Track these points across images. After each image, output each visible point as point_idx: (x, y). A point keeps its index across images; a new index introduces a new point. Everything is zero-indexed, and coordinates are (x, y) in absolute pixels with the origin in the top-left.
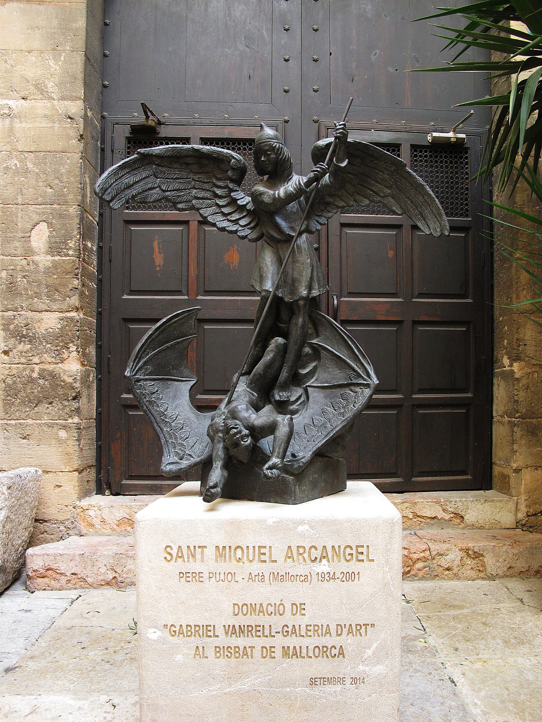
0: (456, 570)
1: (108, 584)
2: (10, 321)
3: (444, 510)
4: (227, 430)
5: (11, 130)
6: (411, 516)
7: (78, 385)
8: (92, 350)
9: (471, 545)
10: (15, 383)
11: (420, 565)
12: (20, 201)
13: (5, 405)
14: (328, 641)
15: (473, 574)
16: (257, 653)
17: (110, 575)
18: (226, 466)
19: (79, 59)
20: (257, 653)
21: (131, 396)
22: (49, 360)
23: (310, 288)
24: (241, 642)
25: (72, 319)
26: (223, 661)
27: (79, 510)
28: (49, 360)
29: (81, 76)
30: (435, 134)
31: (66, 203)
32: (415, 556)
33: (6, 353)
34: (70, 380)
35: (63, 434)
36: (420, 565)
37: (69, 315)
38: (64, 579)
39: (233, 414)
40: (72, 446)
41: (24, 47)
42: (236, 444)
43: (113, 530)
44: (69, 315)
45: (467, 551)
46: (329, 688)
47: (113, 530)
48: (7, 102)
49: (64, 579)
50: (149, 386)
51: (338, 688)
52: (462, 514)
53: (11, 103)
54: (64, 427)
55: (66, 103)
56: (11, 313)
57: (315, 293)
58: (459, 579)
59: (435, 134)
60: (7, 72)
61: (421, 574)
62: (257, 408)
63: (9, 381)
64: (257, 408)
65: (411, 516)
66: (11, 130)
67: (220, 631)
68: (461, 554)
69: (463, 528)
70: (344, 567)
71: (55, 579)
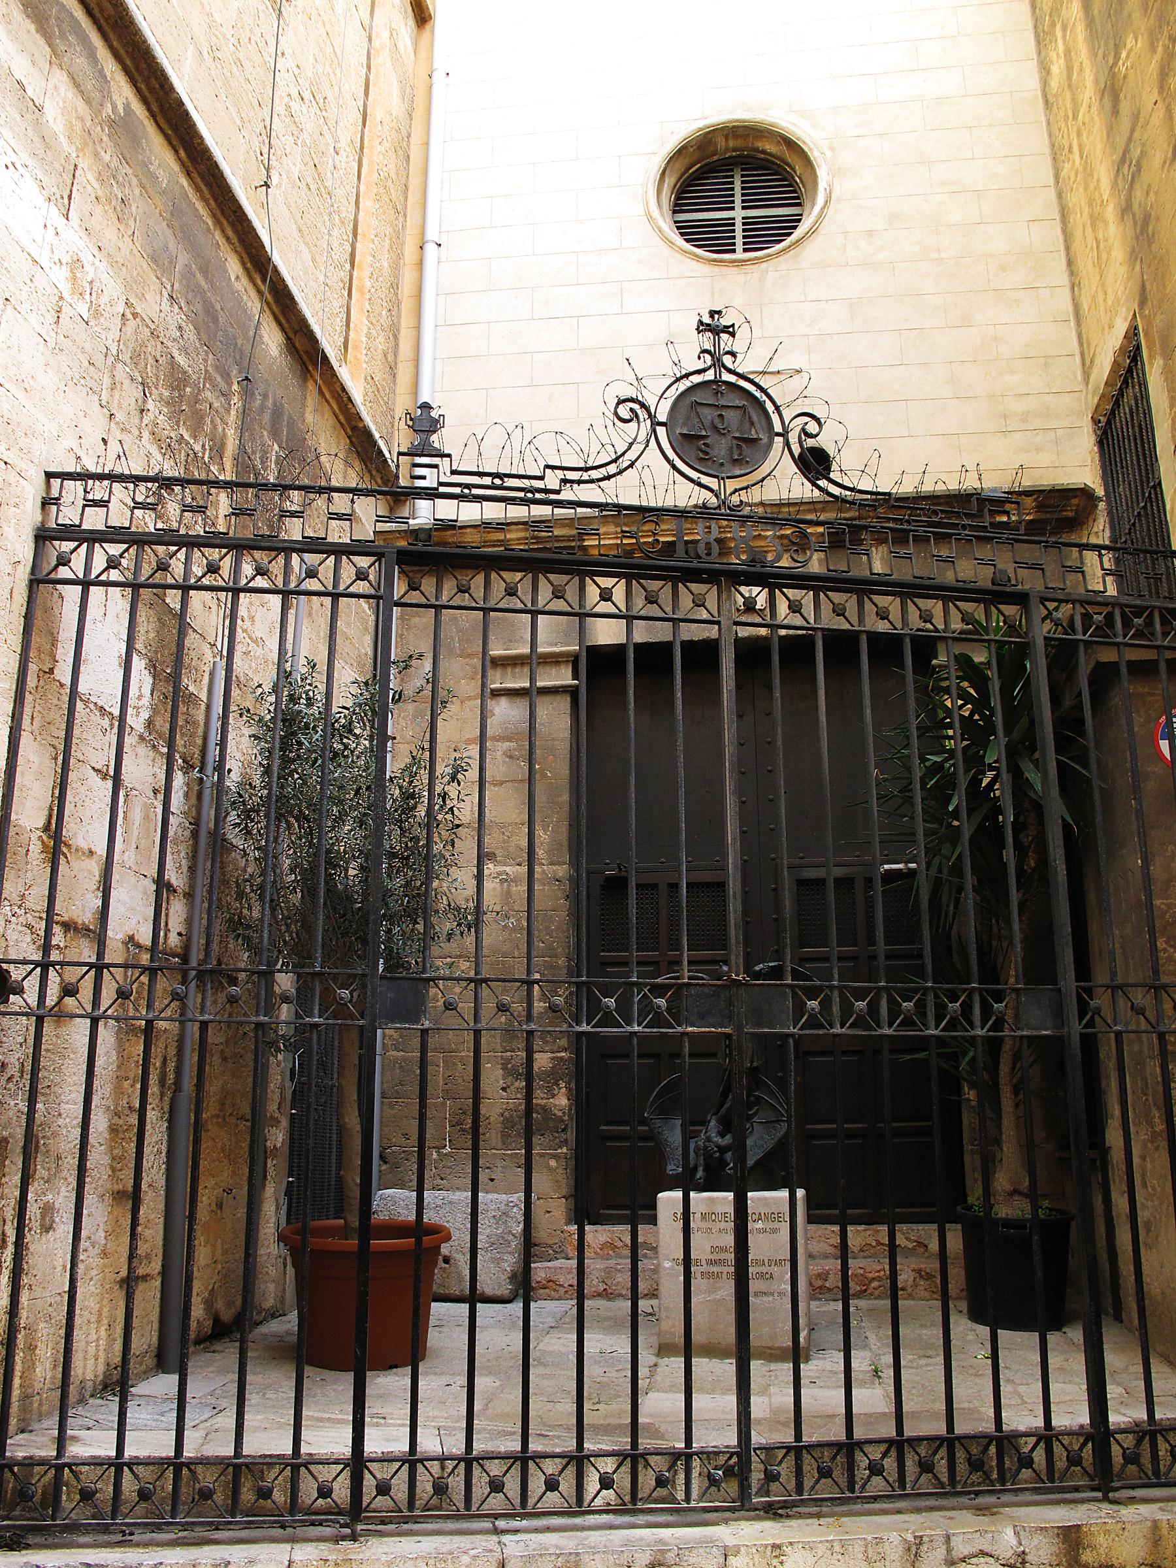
0: (909, 1290)
1: (599, 1295)
2: (508, 1061)
3: (907, 1238)
4: (706, 1147)
5: (508, 892)
6: (874, 1244)
7: (566, 1118)
8: (573, 1085)
9: (923, 1266)
10: (511, 1116)
11: (875, 1284)
12: (516, 954)
13: (503, 1136)
14: (764, 1269)
15: (927, 1295)
16: (724, 1276)
17: (602, 1287)
18: (704, 1170)
19: (564, 829)
20: (724, 1276)
21: (646, 1128)
22: (542, 1095)
23: (752, 1062)
24: (715, 1269)
25: (562, 1058)
26: (705, 1280)
27: (567, 1235)
28: (542, 1095)
29: (566, 843)
30: (886, 867)
31: (556, 956)
32: (870, 1275)
33: (504, 1089)
34: (560, 1114)
35: (553, 1163)
36: (875, 1284)
37: (559, 1055)
38: (562, 1291)
39: (709, 1139)
40: (561, 1175)
41: (518, 820)
42: (711, 1156)
43: (596, 1253)
44: (559, 1055)
45: (919, 1271)
46: (765, 1299)
47: (596, 1253)
48: (505, 868)
49: (562, 1291)
50: (658, 1123)
51: (771, 1298)
52: (926, 1242)
53: (508, 869)
54: (555, 1157)
55: (554, 868)
56: (509, 1054)
57: (755, 1064)
58: (913, 1299)
59: (886, 867)
60: (504, 840)
61: (877, 1293)
62: (723, 1136)
63: (507, 1114)
64: (723, 1136)
65: (874, 1244)
66: (508, 892)
67: (704, 1262)
68: (912, 1275)
69: (928, 1257)
70: (770, 1225)
71: (555, 1290)
